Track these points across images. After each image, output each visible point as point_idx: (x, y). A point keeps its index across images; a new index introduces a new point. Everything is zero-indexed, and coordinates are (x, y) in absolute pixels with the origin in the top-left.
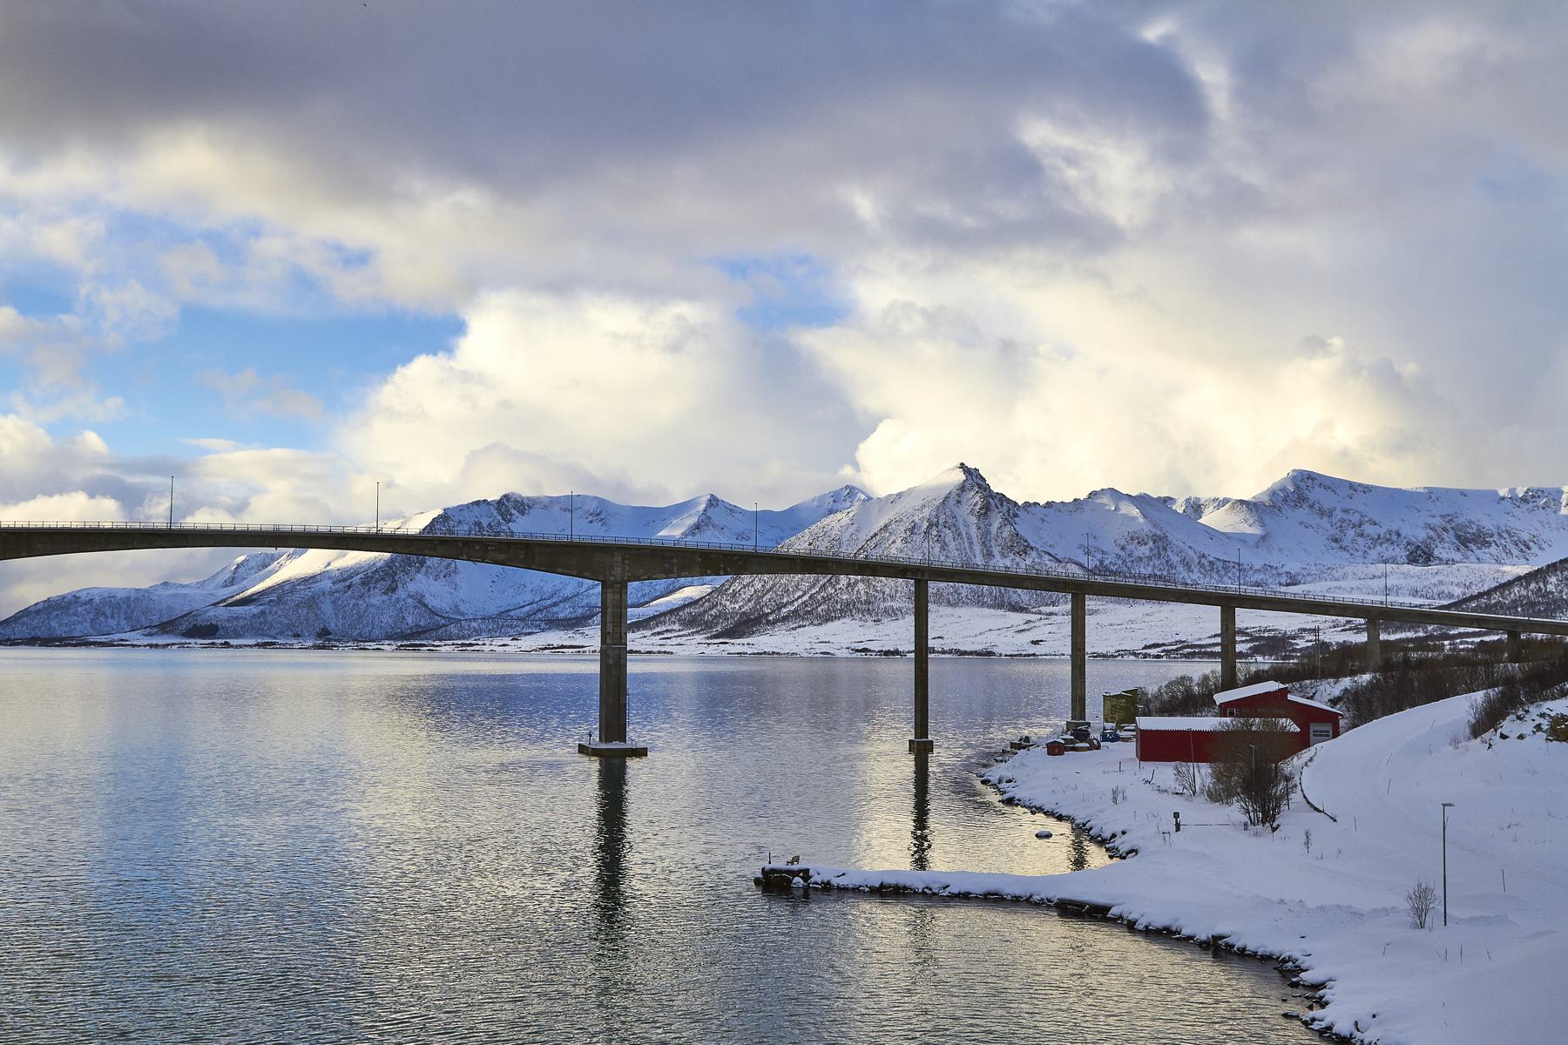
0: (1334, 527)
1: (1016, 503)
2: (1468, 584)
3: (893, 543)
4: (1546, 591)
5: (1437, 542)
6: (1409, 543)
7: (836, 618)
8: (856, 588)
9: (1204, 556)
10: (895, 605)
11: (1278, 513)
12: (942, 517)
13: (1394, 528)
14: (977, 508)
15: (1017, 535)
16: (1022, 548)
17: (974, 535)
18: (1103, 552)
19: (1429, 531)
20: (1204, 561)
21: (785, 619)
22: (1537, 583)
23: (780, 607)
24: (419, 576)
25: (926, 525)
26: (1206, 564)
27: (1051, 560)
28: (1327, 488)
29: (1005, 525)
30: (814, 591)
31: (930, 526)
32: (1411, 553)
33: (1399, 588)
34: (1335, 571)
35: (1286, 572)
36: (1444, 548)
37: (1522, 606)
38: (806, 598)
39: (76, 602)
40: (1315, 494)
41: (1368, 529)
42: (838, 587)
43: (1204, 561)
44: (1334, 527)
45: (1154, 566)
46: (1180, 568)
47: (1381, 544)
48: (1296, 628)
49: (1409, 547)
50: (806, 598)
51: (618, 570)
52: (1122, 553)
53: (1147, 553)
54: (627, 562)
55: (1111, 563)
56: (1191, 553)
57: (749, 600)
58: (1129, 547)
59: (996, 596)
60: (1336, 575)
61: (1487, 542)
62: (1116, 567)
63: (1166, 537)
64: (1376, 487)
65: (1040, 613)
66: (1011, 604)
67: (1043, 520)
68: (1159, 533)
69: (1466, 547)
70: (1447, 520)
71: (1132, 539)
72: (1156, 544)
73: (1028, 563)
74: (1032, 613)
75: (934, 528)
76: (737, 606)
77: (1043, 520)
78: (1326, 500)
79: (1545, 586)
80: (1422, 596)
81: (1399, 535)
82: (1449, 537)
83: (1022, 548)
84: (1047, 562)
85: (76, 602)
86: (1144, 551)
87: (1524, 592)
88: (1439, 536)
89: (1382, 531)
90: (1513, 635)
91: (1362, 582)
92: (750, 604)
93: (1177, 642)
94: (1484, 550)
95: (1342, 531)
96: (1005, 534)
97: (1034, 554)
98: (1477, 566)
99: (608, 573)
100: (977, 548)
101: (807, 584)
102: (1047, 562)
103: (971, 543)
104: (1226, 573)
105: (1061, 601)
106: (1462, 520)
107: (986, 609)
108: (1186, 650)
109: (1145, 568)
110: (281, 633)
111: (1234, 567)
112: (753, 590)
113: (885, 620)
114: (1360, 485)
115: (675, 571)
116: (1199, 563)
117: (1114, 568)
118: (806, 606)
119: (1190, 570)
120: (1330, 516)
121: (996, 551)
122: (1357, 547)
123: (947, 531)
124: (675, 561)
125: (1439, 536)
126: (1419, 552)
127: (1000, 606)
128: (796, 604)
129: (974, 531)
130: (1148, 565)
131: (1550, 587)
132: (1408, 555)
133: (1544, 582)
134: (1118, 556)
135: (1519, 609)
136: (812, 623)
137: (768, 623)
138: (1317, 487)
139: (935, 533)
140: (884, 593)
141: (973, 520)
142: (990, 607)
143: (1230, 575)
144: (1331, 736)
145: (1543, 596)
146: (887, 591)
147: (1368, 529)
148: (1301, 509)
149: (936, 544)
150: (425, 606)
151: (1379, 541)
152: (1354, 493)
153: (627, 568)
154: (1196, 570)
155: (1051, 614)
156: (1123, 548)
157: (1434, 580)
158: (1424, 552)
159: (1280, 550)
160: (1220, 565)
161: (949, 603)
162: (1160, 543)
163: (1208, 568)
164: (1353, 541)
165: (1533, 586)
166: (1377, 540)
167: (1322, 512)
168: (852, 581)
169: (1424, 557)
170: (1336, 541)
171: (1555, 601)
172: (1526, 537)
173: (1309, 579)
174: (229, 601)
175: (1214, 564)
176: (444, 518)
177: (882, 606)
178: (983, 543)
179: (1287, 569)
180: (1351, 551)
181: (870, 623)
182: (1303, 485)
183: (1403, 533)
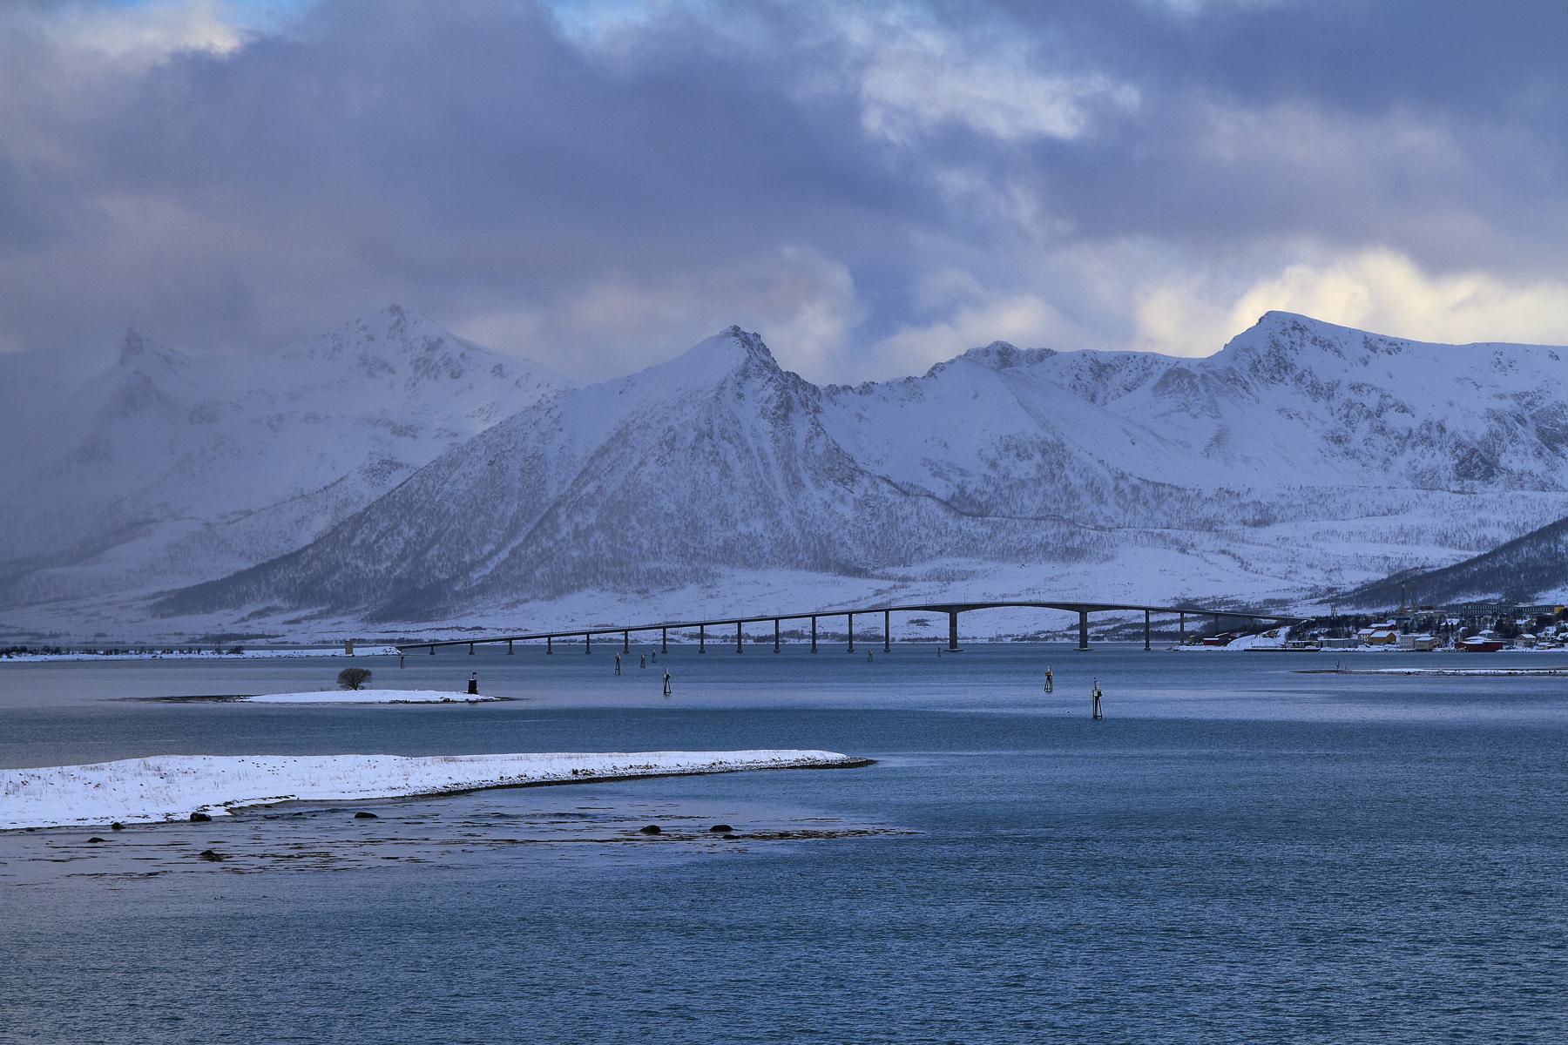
0: (1337, 416)
1: (815, 389)
2: (1521, 525)
3: (641, 464)
4: (1556, 551)
5: (1506, 441)
6: (1459, 445)
7: (573, 588)
8: (592, 540)
9: (1123, 476)
10: (664, 565)
11: (1244, 393)
12: (717, 421)
13: (1437, 418)
14: (771, 407)
15: (838, 450)
16: (848, 472)
17: (769, 451)
18: (962, 472)
19: (1492, 422)
20: (1123, 485)
21: (483, 589)
22: (1549, 543)
23: (465, 570)
25: (692, 435)
27: (893, 492)
28: (1327, 345)
29: (818, 434)
30: (515, 543)
31: (701, 436)
32: (1462, 462)
33: (1421, 533)
34: (1330, 501)
35: (1254, 502)
36: (1516, 452)
38: (504, 555)
40: (1308, 358)
41: (1394, 420)
42: (558, 537)
43: (1123, 485)
44: (1337, 416)
45: (1045, 495)
46: (1086, 498)
47: (1414, 446)
48: (1261, 598)
49: (1458, 452)
50: (504, 555)
52: (992, 474)
53: (1033, 473)
55: (976, 490)
56: (1103, 471)
57: (402, 558)
58: (1003, 463)
59: (815, 552)
60: (1333, 507)
62: (985, 498)
63: (1063, 445)
64: (1409, 343)
65: (889, 578)
66: (840, 564)
67: (860, 417)
68: (1050, 438)
69: (1554, 449)
70: (1524, 402)
71: (1007, 449)
72: (1047, 458)
73: (858, 497)
74: (877, 578)
75: (707, 440)
76: (382, 568)
77: (860, 417)
78: (1323, 366)
79: (1556, 546)
80: (1453, 545)
81: (1442, 429)
82: (1528, 434)
83: (848, 472)
84: (888, 495)
86: (1025, 469)
87: (1532, 554)
88: (1509, 431)
89: (1415, 424)
91: (1369, 521)
92: (405, 565)
93: (1111, 620)
95: (1349, 423)
96: (819, 450)
97: (866, 481)
98: (1539, 495)
100: (777, 474)
101: (500, 532)
102: (888, 495)
103: (766, 465)
104: (1159, 505)
105: (914, 557)
106: (1547, 402)
107: (803, 571)
108: (1126, 630)
109: (1030, 498)
111: (1171, 494)
112: (401, 540)
114: (1382, 339)
116: (1116, 488)
117: (982, 499)
118: (511, 568)
119: (1101, 500)
120: (1330, 397)
121: (806, 477)
122: (1374, 452)
123: (728, 446)
125: (1509, 431)
126: (1475, 460)
127: (824, 566)
128: (491, 565)
129: (768, 445)
130: (1036, 493)
132: (1457, 466)
133: (1555, 542)
134: (987, 478)
135: (1522, 576)
136: (534, 597)
138: (1308, 344)
139: (708, 448)
140: (640, 547)
141: (765, 425)
142: (810, 568)
143: (1165, 508)
144: (1016, 355)
146: (646, 545)
147: (1394, 420)
148: (1282, 385)
149: (712, 466)
151: (1409, 442)
152: (1371, 353)
154: (1111, 501)
155: (905, 579)
156: (993, 465)
157: (1473, 519)
158: (1484, 461)
159: (1246, 460)
160: (1148, 490)
161: (747, 564)
162: (1053, 456)
163: (1129, 497)
164: (1367, 441)
165: (1543, 546)
166: (1407, 439)
167: (1316, 390)
169: (1483, 468)
173: (1290, 513)
175: (1139, 490)
178: (786, 464)
179: (1255, 496)
180: (1363, 459)
181: (632, 596)
182: (1285, 340)
183: (1450, 426)
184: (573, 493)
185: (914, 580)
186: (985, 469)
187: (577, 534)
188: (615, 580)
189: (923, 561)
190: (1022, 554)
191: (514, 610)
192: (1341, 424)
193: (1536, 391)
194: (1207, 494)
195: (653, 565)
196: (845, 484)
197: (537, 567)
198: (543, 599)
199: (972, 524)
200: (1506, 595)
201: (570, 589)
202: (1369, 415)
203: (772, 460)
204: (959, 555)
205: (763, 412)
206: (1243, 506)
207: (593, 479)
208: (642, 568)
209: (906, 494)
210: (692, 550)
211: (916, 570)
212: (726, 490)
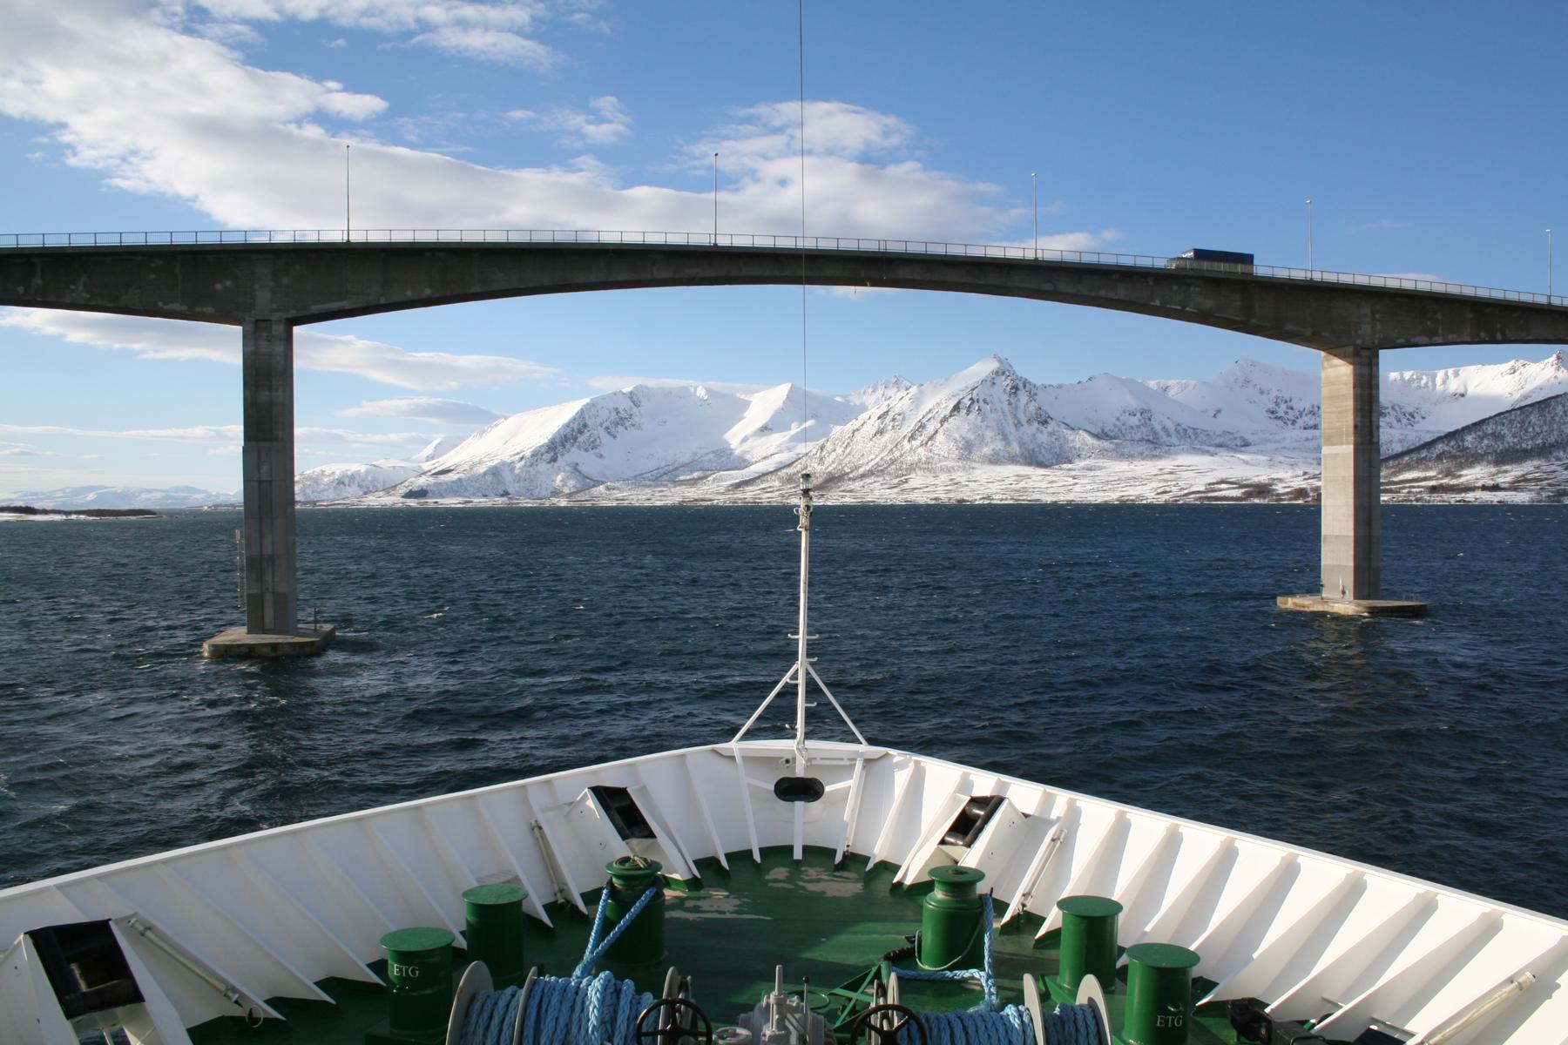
9: (1178, 425)
14: (1008, 389)
20: (1179, 428)
23: (857, 468)
24: (573, 449)
38: (878, 459)
39: (323, 475)
43: (1179, 428)
51: (1366, 329)
54: (1378, 316)
57: (833, 462)
58: (1122, 418)
71: (1124, 412)
85: (323, 475)
99: (1353, 333)
100: (1010, 420)
104: (1196, 438)
110: (474, 494)
115: (1440, 331)
117: (1112, 434)
124: (1439, 316)
131: (1466, 444)
134: (1115, 426)
137: (850, 479)
145: (1461, 451)
150: (579, 472)
153: (1379, 327)
164: (1286, 413)
165: (1453, 443)
170: (1272, 413)
172: (1410, 409)
174: (434, 471)
176: (482, 432)
186: (1114, 421)
192: (1274, 405)
193: (1171, 427)
194: (1218, 433)
202: (1286, 402)
203: (1008, 414)
206: (1236, 438)
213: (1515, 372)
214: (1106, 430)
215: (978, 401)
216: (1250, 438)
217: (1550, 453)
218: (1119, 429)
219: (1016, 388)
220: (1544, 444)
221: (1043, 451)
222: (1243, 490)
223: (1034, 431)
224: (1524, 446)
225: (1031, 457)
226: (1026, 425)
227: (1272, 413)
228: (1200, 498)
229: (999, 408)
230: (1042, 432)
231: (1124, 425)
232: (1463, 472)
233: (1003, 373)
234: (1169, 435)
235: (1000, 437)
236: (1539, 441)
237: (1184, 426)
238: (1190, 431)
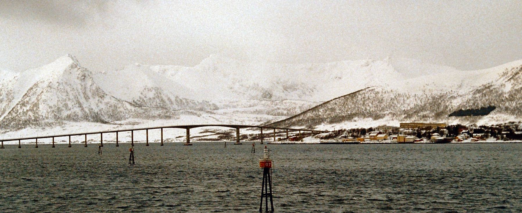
2: (289, 109)
6: (263, 89)
7: (22, 128)
14: (80, 76)
26: (179, 100)
32: (263, 94)
37: (310, 120)
58: (144, 93)
61: (295, 89)
65: (116, 124)
79: (318, 113)
82: (280, 87)
90: (312, 132)
94: (294, 92)
96: (94, 88)
113: (47, 128)
127: (97, 121)
131: (320, 113)
134: (140, 98)
135: (310, 121)
136: (11, 130)
141: (79, 81)
146: (44, 116)
157: (276, 108)
158: (269, 94)
165: (314, 113)
168: (25, 111)
171: (321, 119)
177: (18, 74)
184: (22, 101)
185: (123, 125)
186: (139, 95)
187: (24, 112)
188: (35, 125)
189: (125, 119)
190: (154, 117)
191: (5, 134)
193: (173, 99)
195: (46, 121)
196: (102, 98)
197: (12, 122)
198: (14, 131)
199: (138, 109)
200: (306, 127)
201: (21, 128)
204: (135, 118)
205: (78, 78)
207: (28, 96)
208: (43, 122)
209: (119, 101)
210: (58, 117)
211: (122, 122)
212: (67, 99)
213: (368, 65)
214: (136, 100)
215: (62, 83)
216: (218, 104)
217: (353, 118)
218: (143, 100)
219: (84, 76)
220: (351, 113)
221: (103, 113)
222: (218, 135)
223: (97, 102)
224: (343, 114)
225: (96, 117)
226: (91, 98)
227: (231, 88)
228: (200, 140)
229: (75, 88)
230: (101, 102)
231: (145, 97)
232: (316, 127)
233: (76, 67)
234: (172, 103)
235: (77, 105)
236: (349, 112)
237: (181, 97)
238: (184, 101)
